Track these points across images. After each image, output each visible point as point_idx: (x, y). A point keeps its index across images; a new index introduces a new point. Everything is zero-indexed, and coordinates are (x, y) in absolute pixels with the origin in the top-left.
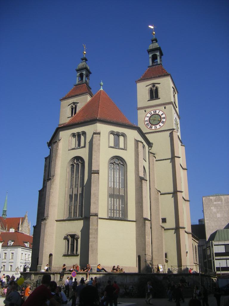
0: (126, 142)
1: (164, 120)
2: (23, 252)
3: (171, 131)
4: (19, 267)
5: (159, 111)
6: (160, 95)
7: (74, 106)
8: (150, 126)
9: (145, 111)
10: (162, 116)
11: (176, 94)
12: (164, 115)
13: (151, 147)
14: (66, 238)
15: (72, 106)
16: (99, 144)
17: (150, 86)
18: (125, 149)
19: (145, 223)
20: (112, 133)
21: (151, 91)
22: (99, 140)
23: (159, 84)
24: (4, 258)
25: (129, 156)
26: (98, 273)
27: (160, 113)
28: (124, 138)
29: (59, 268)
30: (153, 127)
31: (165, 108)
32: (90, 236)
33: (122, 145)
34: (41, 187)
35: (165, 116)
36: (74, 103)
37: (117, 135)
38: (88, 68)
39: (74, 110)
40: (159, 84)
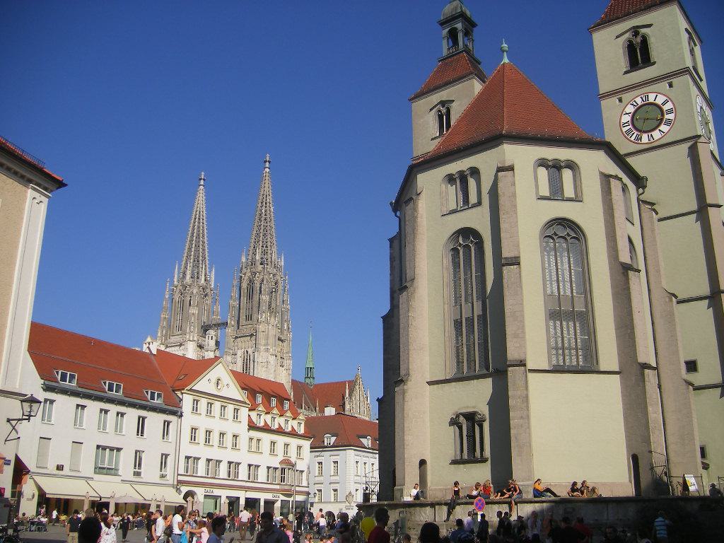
0: (578, 183)
1: (671, 116)
2: (358, 458)
3: (692, 143)
4: (353, 492)
5: (655, 94)
6: (654, 55)
7: (444, 110)
9: (620, 100)
10: (665, 108)
11: (695, 45)
13: (644, 187)
14: (454, 422)
15: (440, 111)
16: (514, 195)
17: (627, 35)
18: (577, 199)
19: (643, 375)
20: (543, 163)
21: (631, 48)
22: (514, 184)
23: (649, 26)
24: (317, 474)
25: (589, 215)
26: (536, 499)
27: (660, 100)
28: (573, 173)
29: (444, 491)
30: (645, 138)
31: (671, 85)
32: (512, 414)
33: (569, 191)
34: (386, 309)
35: (672, 106)
36: (443, 103)
37: (555, 167)
38: (468, 13)
39: (444, 118)
40: (649, 26)
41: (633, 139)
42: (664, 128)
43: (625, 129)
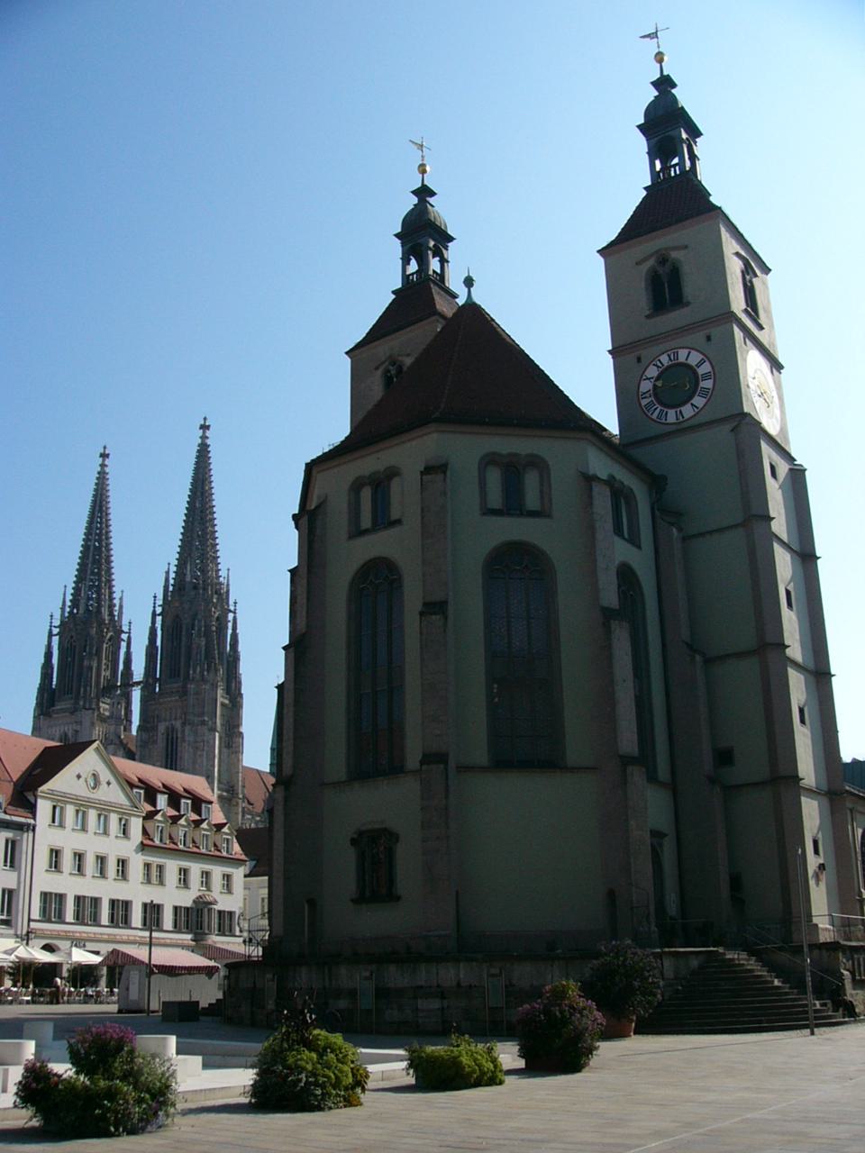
1: (708, 384)
6: (689, 290)
8: (658, 410)
12: (707, 364)
14: (354, 842)
15: (389, 371)
17: (651, 262)
27: (694, 359)
30: (672, 416)
41: (654, 416)
42: (698, 401)
43: (644, 402)
